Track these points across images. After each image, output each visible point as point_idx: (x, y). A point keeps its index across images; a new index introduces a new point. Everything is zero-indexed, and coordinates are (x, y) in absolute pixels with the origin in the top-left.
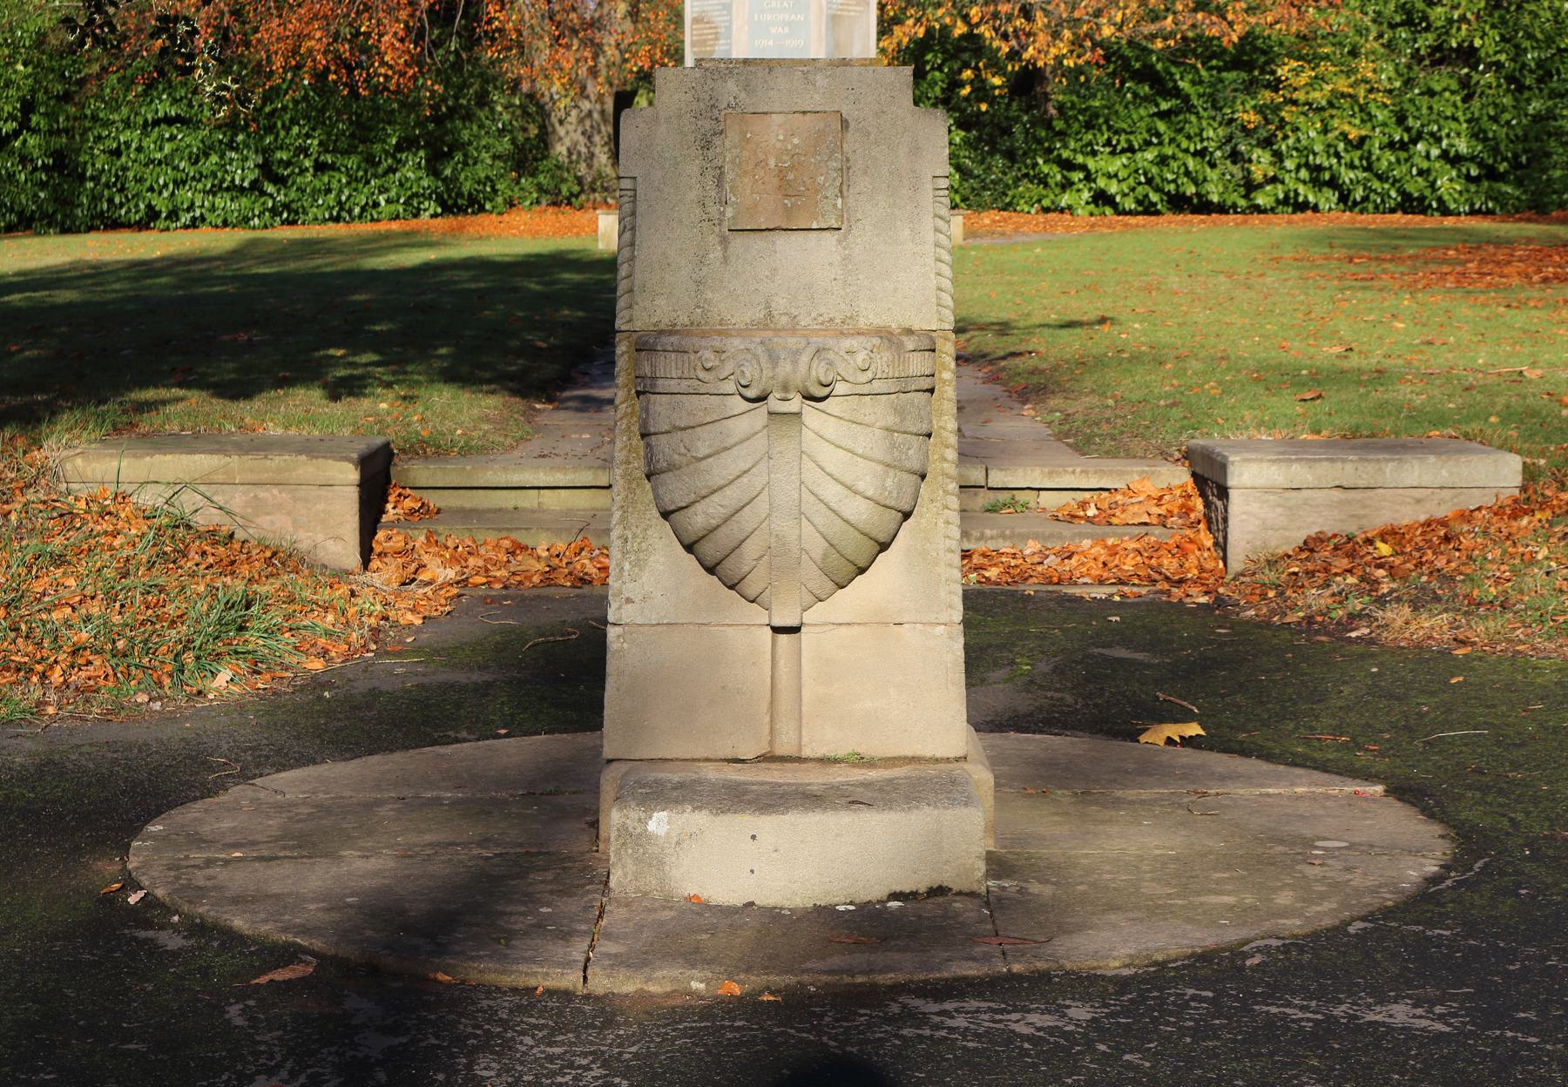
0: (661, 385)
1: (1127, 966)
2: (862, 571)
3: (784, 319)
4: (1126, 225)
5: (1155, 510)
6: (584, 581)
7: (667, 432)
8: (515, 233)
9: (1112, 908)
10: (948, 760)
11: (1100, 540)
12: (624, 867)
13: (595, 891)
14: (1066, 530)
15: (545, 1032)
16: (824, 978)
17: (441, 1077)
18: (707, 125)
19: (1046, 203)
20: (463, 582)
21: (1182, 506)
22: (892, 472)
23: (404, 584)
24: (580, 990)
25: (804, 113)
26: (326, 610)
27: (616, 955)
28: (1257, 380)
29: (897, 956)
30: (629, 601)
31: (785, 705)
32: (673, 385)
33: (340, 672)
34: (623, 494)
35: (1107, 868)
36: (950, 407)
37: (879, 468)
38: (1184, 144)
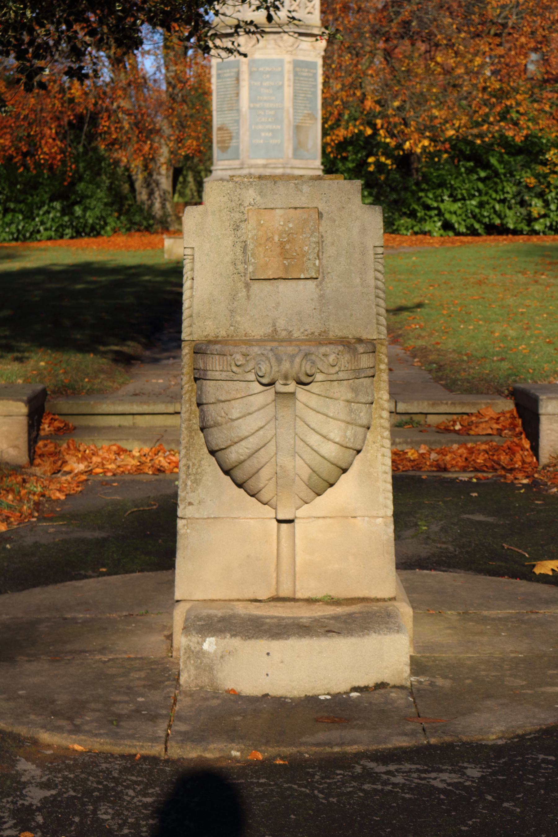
0: (210, 374)
1: (501, 738)
2: (331, 485)
3: (284, 333)
4: (461, 242)
5: (496, 426)
6: (160, 470)
7: (213, 403)
8: (117, 250)
9: (488, 696)
10: (384, 600)
11: (463, 444)
12: (188, 671)
13: (171, 686)
14: (444, 438)
15: (141, 787)
16: (315, 749)
17: (77, 819)
18: (237, 216)
19: (416, 229)
20: (89, 472)
21: (511, 424)
22: (350, 427)
23: (54, 473)
24: (163, 756)
25: (296, 208)
26: (8, 492)
27: (185, 733)
28: (549, 342)
29: (358, 733)
30: (190, 504)
31: (285, 566)
32: (217, 375)
33: (16, 531)
34: (186, 439)
35: (483, 667)
36: (385, 386)
37: (343, 425)
38: (494, 195)
